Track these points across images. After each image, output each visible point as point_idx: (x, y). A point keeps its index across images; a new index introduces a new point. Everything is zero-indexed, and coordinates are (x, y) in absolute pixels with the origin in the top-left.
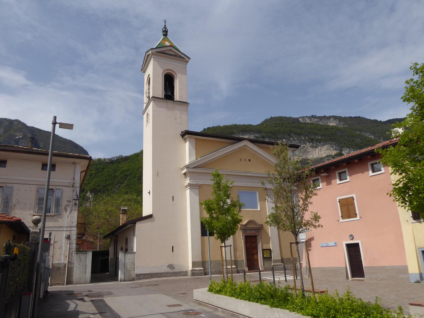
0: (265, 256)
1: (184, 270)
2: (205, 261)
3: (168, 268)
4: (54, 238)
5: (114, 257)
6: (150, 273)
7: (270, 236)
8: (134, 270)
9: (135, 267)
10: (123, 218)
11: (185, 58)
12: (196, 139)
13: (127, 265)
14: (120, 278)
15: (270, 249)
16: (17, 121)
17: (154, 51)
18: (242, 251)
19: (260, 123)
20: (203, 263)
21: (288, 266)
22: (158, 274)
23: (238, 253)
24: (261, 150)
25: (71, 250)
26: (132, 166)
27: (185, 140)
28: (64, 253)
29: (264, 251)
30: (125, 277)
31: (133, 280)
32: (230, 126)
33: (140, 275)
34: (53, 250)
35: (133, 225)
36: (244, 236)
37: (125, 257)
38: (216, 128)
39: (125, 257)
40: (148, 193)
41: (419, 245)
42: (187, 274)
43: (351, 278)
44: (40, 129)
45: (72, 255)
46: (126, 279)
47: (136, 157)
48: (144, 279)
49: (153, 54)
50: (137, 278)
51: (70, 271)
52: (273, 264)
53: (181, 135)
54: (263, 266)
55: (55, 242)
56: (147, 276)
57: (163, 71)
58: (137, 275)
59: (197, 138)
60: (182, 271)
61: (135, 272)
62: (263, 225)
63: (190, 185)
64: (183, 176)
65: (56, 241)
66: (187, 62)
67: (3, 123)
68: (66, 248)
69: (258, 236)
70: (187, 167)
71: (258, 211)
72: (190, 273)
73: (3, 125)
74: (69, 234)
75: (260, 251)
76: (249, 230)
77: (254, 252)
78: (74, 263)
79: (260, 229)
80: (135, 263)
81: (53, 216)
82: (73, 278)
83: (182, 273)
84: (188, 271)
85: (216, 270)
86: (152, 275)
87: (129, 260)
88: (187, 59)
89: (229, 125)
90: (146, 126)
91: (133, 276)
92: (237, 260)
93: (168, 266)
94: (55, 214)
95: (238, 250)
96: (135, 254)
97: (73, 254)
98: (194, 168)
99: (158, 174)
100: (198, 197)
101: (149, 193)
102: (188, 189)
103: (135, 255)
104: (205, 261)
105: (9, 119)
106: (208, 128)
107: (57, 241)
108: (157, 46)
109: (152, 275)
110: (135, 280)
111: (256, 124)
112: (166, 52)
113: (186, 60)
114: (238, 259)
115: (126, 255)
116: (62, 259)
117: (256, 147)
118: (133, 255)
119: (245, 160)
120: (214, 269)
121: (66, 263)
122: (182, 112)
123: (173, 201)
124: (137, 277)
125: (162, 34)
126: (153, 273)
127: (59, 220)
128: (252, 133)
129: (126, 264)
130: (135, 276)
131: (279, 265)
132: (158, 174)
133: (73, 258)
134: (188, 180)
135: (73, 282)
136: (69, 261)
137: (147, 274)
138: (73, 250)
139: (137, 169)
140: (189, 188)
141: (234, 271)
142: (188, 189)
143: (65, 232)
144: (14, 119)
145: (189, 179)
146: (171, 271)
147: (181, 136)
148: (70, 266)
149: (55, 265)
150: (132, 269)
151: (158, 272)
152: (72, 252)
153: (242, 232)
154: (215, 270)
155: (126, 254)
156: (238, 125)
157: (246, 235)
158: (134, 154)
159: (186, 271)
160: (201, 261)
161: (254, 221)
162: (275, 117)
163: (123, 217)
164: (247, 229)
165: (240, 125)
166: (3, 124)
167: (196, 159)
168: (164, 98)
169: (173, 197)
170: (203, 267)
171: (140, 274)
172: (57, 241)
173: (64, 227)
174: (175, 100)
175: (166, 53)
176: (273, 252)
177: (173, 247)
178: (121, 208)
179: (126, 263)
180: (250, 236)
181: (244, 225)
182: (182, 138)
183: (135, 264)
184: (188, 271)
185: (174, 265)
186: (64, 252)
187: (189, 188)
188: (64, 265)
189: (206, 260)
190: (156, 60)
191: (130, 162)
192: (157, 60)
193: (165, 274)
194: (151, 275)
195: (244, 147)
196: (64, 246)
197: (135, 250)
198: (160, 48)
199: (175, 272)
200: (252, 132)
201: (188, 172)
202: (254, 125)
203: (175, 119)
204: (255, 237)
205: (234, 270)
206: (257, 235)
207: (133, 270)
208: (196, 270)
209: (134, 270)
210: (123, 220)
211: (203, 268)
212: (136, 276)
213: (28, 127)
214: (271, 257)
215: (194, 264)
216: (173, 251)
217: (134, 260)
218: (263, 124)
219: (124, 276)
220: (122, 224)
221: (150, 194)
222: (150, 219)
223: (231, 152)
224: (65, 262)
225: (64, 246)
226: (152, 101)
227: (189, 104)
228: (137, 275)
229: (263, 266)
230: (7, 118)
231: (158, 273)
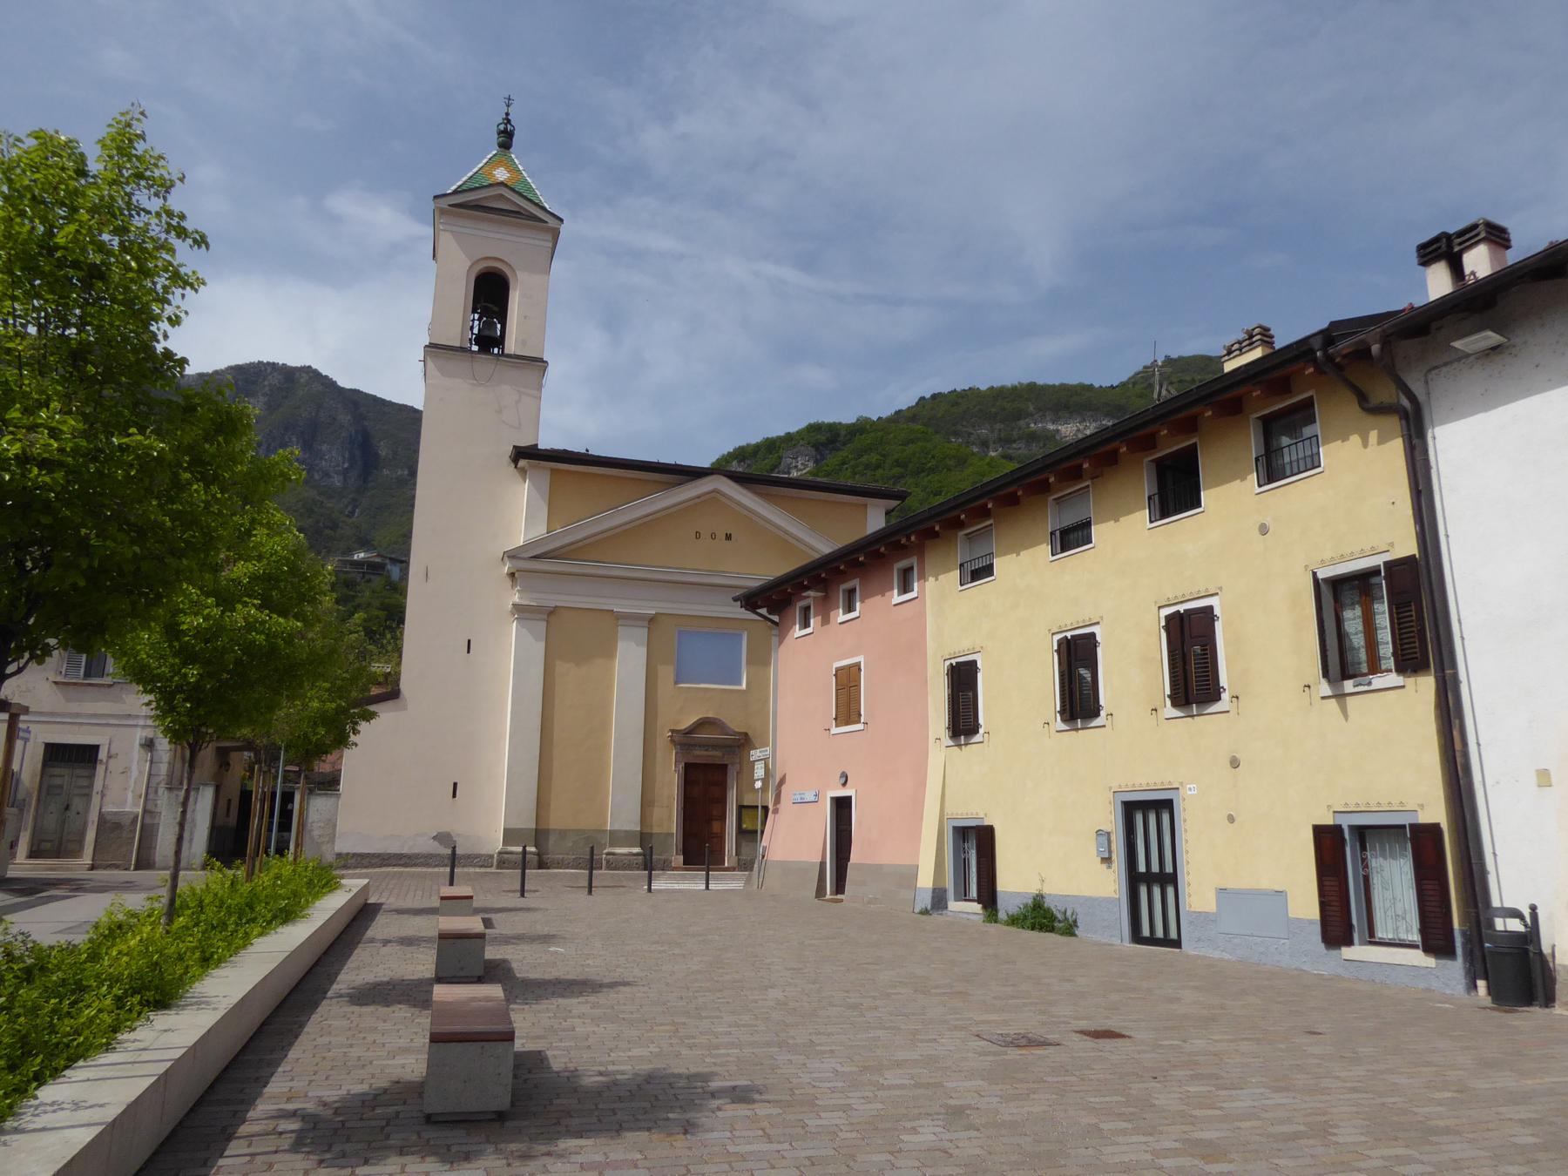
0: (744, 826)
1: (482, 852)
2: (548, 830)
4: (110, 744)
8: (332, 840)
12: (553, 470)
16: (308, 370)
18: (669, 807)
19: (1124, 378)
20: (540, 835)
23: (657, 813)
24: (766, 505)
25: (154, 781)
28: (134, 787)
29: (744, 811)
32: (1014, 388)
34: (105, 776)
36: (681, 766)
38: (963, 397)
41: (951, 810)
43: (831, 895)
44: (379, 396)
45: (156, 792)
51: (148, 834)
55: (110, 757)
56: (368, 859)
57: (469, 264)
58: (339, 855)
63: (518, 608)
64: (508, 582)
65: (113, 751)
67: (264, 380)
68: (141, 772)
69: (729, 767)
73: (265, 386)
74: (151, 736)
77: (715, 813)
78: (160, 816)
81: (110, 686)
82: (155, 853)
88: (552, 222)
89: (1010, 386)
92: (652, 834)
93: (434, 838)
94: (115, 680)
97: (161, 791)
100: (542, 645)
104: (546, 827)
105: (283, 364)
106: (934, 396)
107: (117, 754)
108: (459, 187)
111: (1106, 384)
112: (490, 205)
114: (656, 830)
116: (126, 802)
117: (750, 495)
119: (713, 536)
120: (573, 854)
122: (522, 390)
125: (494, 139)
127: (124, 696)
128: (1092, 416)
129: (309, 825)
133: (159, 802)
135: (154, 863)
136: (148, 807)
138: (162, 777)
141: (635, 862)
143: (139, 729)
144: (298, 364)
148: (148, 820)
149: (109, 818)
151: (405, 851)
152: (158, 784)
153: (676, 753)
154: (574, 857)
156: (1042, 386)
160: (534, 827)
162: (1181, 359)
164: (695, 745)
165: (1049, 386)
166: (266, 383)
169: (469, 641)
171: (348, 854)
172: (117, 754)
173: (137, 717)
175: (492, 208)
180: (705, 765)
183: (335, 825)
185: (452, 833)
186: (135, 783)
188: (132, 816)
189: (550, 827)
190: (452, 231)
192: (454, 228)
196: (134, 767)
198: (471, 190)
200: (1091, 413)
202: (1101, 387)
204: (723, 768)
207: (328, 842)
208: (511, 853)
209: (333, 842)
213: (342, 391)
215: (510, 835)
216: (454, 795)
217: (336, 814)
218: (1134, 384)
224: (135, 810)
225: (134, 767)
229: (734, 854)
230: (276, 362)
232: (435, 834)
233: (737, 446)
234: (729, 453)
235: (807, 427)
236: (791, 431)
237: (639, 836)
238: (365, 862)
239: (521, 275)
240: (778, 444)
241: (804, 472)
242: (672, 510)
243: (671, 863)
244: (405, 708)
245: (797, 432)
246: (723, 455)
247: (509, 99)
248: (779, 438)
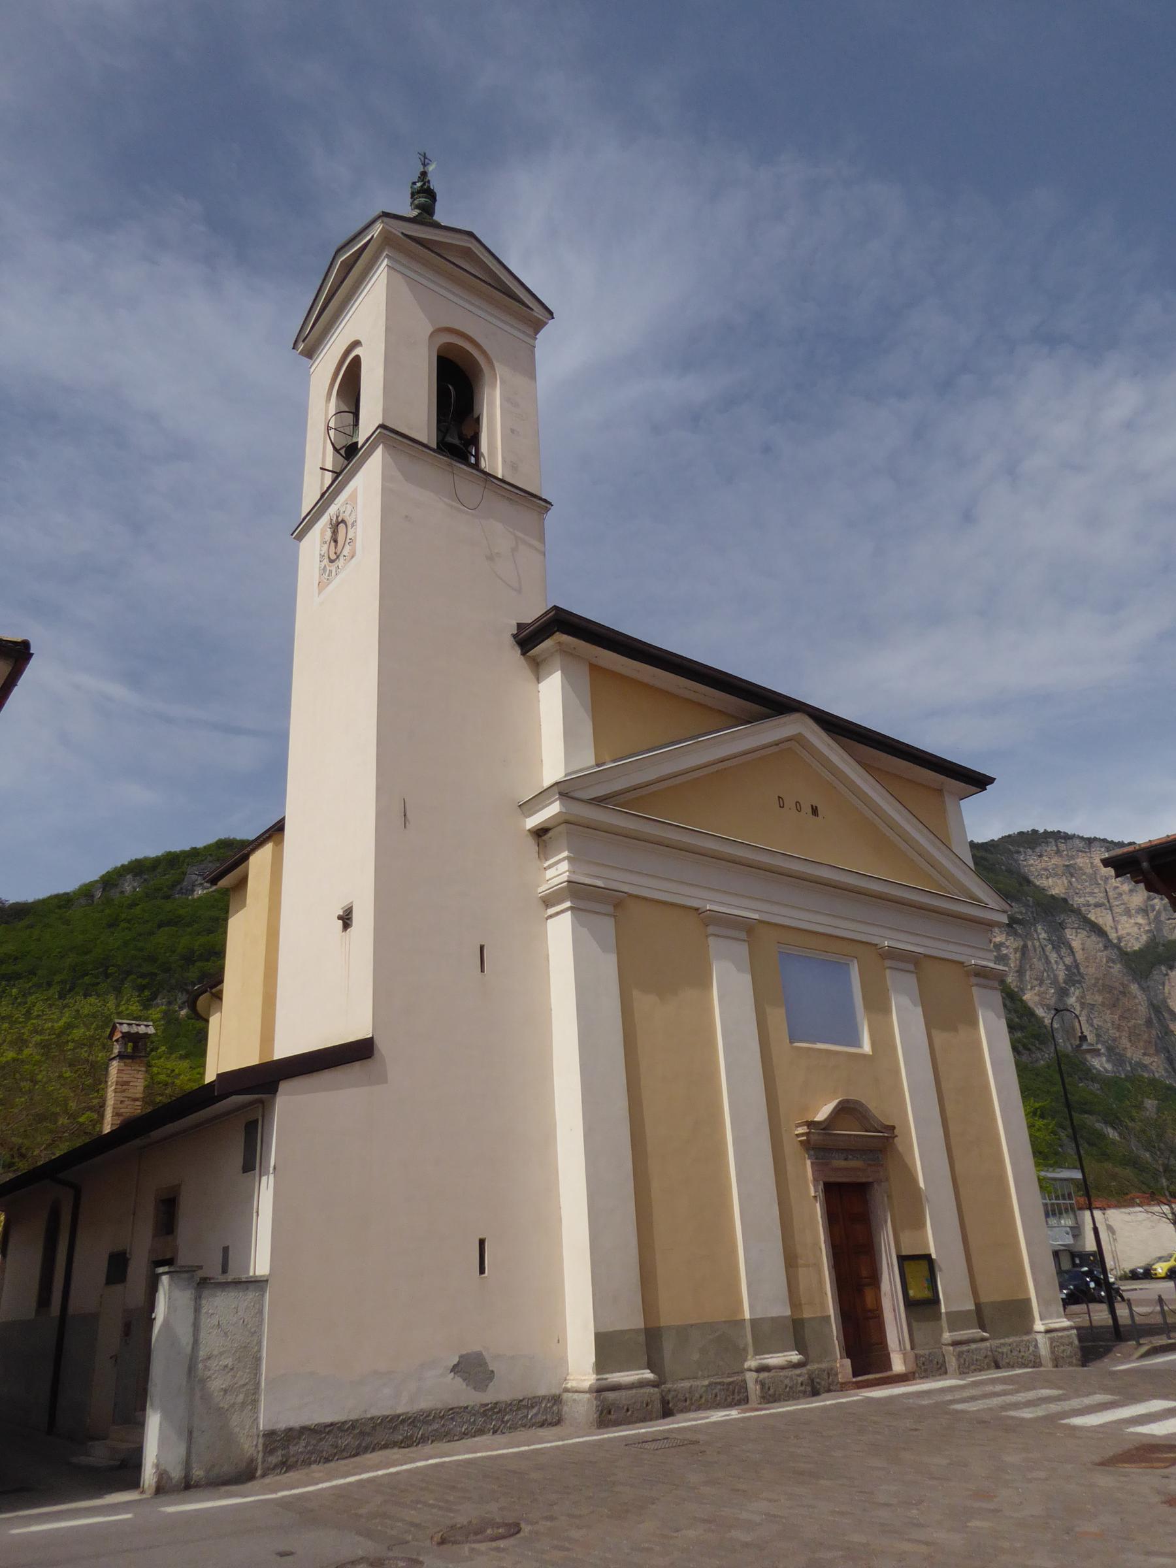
0: (911, 1293)
1: (542, 1392)
2: (659, 1328)
3: (459, 1380)
5: (38, 1312)
6: (353, 1416)
7: (922, 1185)
9: (259, 1383)
10: (122, 1085)
11: (533, 308)
13: (206, 1368)
14: (157, 1466)
15: (928, 1257)
17: (398, 228)
18: (818, 1267)
21: (1004, 1345)
22: (403, 1421)
26: (39, 940)
27: (538, 668)
30: (194, 1458)
31: (245, 1475)
33: (292, 1435)
35: (251, 1103)
36: (821, 1187)
37: (197, 1310)
39: (197, 1310)
40: (340, 918)
42: (559, 1413)
46: (198, 1473)
47: (60, 907)
48: (315, 1462)
49: (387, 240)
50: (273, 1459)
52: (947, 1336)
53: (514, 636)
54: (912, 1348)
56: (331, 1439)
57: (431, 330)
58: (270, 1435)
59: (596, 666)
60: (530, 1396)
61: (257, 1419)
62: (893, 1128)
64: (531, 844)
66: (537, 326)
69: (876, 1186)
70: (563, 790)
71: (864, 1056)
72: (581, 1408)
75: (890, 1265)
76: (838, 1150)
79: (881, 1151)
80: (259, 1351)
83: (535, 1411)
84: (566, 1396)
85: (710, 1384)
86: (362, 1434)
87: (226, 1334)
88: (538, 312)
90: (322, 586)
91: (246, 1446)
93: (455, 1369)
95: (801, 1262)
96: (263, 1291)
98: (598, 801)
99: (405, 815)
101: (346, 920)
102: (562, 912)
103: (263, 1295)
109: (362, 1434)
110: (259, 1473)
113: (533, 313)
114: (806, 1315)
115: (204, 1302)
118: (251, 1295)
120: (704, 1377)
123: (482, 970)
124: (269, 1450)
126: (369, 1416)
129: (200, 1366)
130: (260, 1448)
131: (974, 1341)
132: (408, 814)
134: (564, 866)
137: (332, 1424)
139: (60, 952)
140: (568, 904)
141: (800, 1379)
142: (562, 912)
145: (567, 858)
146: (471, 1397)
147: (516, 641)
150: (241, 1397)
154: (706, 1382)
155: (206, 1293)
157: (832, 1180)
158: (51, 898)
159: (555, 1391)
160: (642, 1326)
161: (861, 1104)
163: (126, 1078)
167: (598, 765)
169: (482, 948)
170: (651, 1367)
176: (941, 1270)
177: (482, 1243)
178: (121, 1024)
179: (202, 1354)
181: (822, 1127)
182: (524, 653)
183: (258, 1360)
184: (567, 1390)
187: (568, 904)
189: (662, 1325)
191: (31, 926)
193: (442, 1418)
194: (357, 1431)
197: (261, 1264)
199: (496, 1404)
201: (566, 822)
203: (490, 558)
205: (799, 1375)
206: (870, 1180)
209: (255, 1402)
210: (124, 1091)
211: (652, 1372)
212: (265, 1446)
214: (935, 1301)
216: (482, 1270)
217: (257, 1333)
219: (182, 1450)
220: (117, 1114)
222: (355, 1070)
223: (763, 753)
226: (381, 446)
227: (549, 506)
228: (277, 1440)
231: (399, 1416)
232: (455, 1360)
233: (134, 859)
234: (123, 866)
235: (216, 843)
236: (198, 847)
237: (791, 1327)
238: (326, 1446)
239: (500, 369)
240: (181, 859)
241: (211, 890)
242: (678, 781)
243: (836, 1375)
244: (383, 1079)
245: (205, 847)
246: (116, 868)
247: (425, 158)
248: (183, 852)
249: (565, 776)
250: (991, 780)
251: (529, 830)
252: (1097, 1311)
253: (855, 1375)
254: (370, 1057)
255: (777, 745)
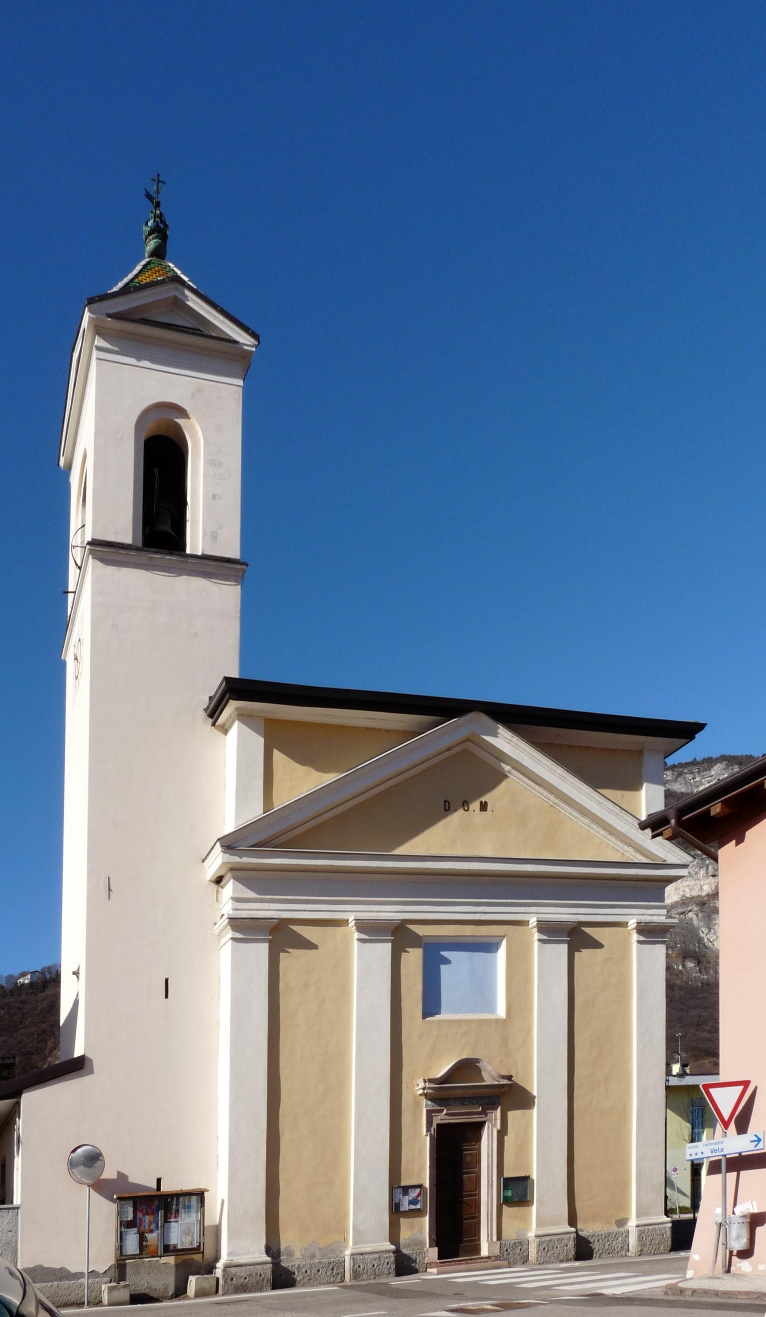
70: (229, 844)
71: (497, 1021)
80: (16, 1245)
121: (484, 1081)
168: (140, 544)
169: (167, 981)
174: (188, 551)
195: (468, 745)
197: (17, 1200)
221: (78, 977)
249: (235, 828)
250: (700, 727)
251: (209, 881)
252: (17, 1201)
253: (438, 1259)
254: (83, 1068)
255: (448, 750)
